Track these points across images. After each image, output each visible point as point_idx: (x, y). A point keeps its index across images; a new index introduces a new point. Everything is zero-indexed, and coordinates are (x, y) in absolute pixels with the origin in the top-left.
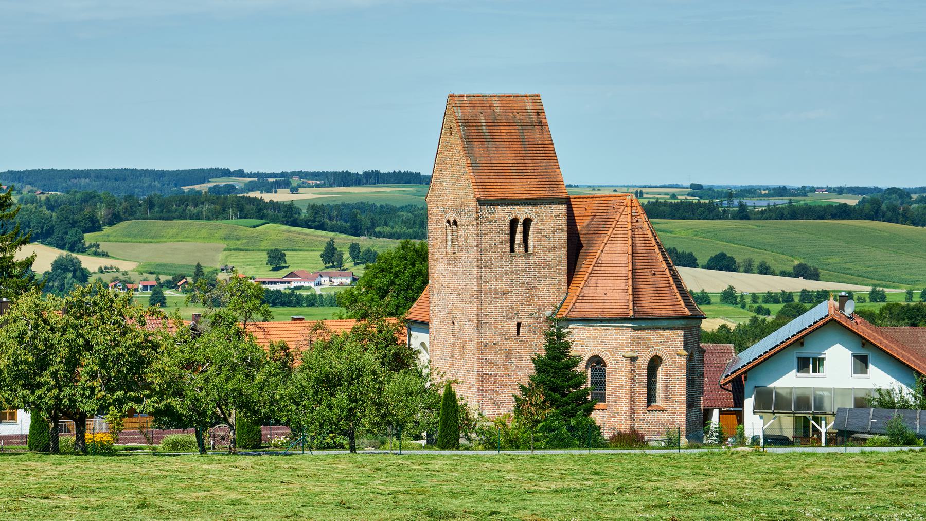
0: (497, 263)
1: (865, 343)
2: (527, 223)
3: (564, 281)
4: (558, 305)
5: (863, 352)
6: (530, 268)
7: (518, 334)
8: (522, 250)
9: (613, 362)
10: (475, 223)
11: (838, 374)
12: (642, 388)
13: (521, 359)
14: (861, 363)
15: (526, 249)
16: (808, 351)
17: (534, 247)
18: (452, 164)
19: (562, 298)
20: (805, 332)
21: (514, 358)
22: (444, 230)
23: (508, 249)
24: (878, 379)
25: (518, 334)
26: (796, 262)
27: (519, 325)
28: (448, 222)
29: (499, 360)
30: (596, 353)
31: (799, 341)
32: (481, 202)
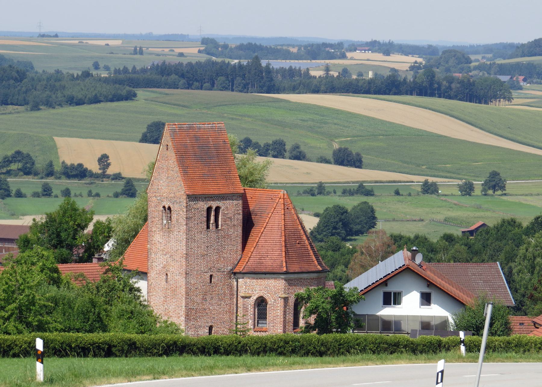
0: (198, 237)
1: (430, 284)
2: (218, 209)
3: (240, 247)
4: (236, 262)
5: (427, 290)
6: (219, 239)
7: (211, 282)
8: (214, 227)
9: (272, 301)
10: (185, 210)
11: (411, 306)
12: (290, 317)
13: (212, 298)
14: (426, 299)
15: (217, 226)
16: (392, 288)
17: (222, 226)
18: (168, 169)
19: (238, 258)
20: (388, 277)
21: (208, 297)
22: (161, 213)
23: (206, 227)
24: (437, 311)
25: (211, 282)
26: (336, 146)
27: (211, 276)
28: (164, 207)
29: (198, 299)
30: (262, 294)
31: (385, 282)
32: (189, 196)
